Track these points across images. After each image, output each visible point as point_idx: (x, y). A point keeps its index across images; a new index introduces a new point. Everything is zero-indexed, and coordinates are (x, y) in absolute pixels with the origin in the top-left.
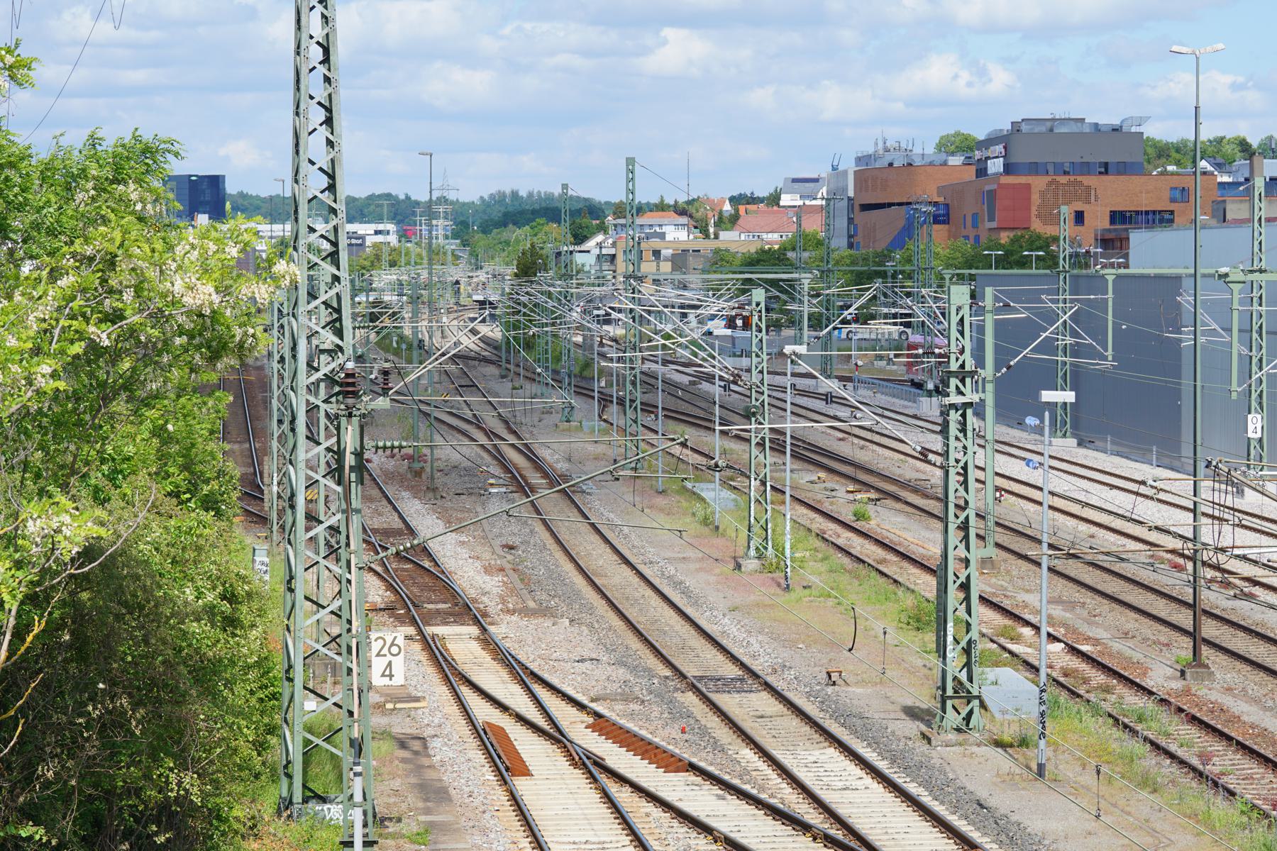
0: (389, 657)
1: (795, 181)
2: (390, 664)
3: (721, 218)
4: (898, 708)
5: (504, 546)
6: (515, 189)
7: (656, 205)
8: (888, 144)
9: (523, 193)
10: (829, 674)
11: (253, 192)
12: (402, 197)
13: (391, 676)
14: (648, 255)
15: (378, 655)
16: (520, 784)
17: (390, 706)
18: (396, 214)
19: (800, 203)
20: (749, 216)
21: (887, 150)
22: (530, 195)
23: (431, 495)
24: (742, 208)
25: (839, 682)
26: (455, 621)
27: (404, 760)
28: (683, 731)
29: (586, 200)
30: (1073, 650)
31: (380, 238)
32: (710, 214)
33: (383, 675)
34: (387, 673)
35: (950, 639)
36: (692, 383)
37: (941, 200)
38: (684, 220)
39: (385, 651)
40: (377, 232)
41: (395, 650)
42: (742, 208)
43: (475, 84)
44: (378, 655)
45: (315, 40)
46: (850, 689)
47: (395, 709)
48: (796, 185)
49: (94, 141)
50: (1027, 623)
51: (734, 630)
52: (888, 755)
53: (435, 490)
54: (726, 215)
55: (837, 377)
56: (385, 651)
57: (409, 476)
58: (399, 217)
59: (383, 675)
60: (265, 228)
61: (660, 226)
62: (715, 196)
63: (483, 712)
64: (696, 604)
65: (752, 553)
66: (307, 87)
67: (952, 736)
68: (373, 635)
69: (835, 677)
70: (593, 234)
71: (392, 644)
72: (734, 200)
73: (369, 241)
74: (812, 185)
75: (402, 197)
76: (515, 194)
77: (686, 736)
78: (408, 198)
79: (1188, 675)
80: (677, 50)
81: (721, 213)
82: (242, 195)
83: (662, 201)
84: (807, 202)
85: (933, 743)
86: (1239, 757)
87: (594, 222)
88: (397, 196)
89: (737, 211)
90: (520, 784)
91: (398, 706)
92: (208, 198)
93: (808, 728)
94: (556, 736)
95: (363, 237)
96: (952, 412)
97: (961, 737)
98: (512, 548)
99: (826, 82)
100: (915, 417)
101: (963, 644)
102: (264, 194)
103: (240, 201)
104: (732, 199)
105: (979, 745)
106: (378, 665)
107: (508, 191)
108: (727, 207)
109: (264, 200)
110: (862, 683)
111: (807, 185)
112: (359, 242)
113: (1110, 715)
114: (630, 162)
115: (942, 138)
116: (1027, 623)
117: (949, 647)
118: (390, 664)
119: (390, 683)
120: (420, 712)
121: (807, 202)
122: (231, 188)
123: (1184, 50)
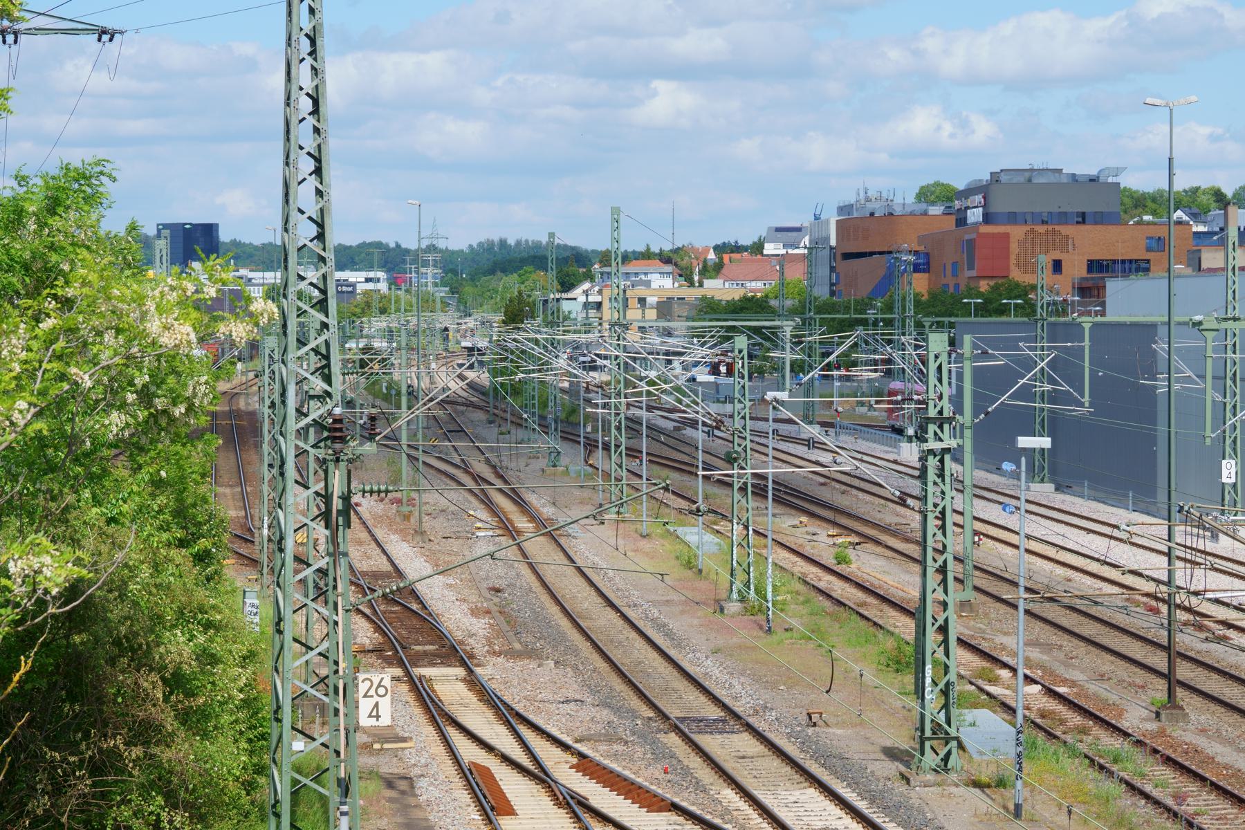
0: (376, 699)
1: (778, 230)
2: (377, 705)
4: (878, 749)
6: (503, 236)
8: (869, 194)
9: (511, 242)
10: (809, 716)
11: (246, 240)
12: (392, 245)
13: (378, 717)
14: (633, 303)
15: (365, 696)
16: (575, 760)
17: (377, 746)
19: (784, 252)
21: (868, 200)
22: (518, 243)
23: (419, 538)
24: (726, 257)
25: (820, 723)
26: (442, 663)
28: (666, 772)
29: (573, 248)
30: (1051, 692)
31: (370, 286)
32: (695, 262)
33: (370, 716)
34: (374, 713)
36: (677, 429)
37: (921, 248)
38: (669, 268)
39: (372, 692)
40: (368, 280)
41: (381, 691)
42: (726, 257)
43: (466, 134)
44: (365, 696)
46: (830, 730)
47: (382, 749)
48: (779, 235)
51: (716, 672)
54: (710, 263)
55: (819, 423)
56: (372, 692)
57: (398, 519)
58: (389, 265)
59: (370, 716)
61: (646, 274)
62: (699, 244)
63: (469, 752)
64: (679, 646)
65: (735, 596)
66: (297, 137)
67: (930, 777)
68: (361, 676)
69: (815, 718)
71: (379, 685)
72: (719, 249)
73: (360, 288)
74: (795, 234)
75: (392, 245)
76: (503, 243)
77: (669, 777)
78: (398, 246)
79: (1163, 717)
80: (666, 102)
81: (705, 261)
83: (648, 249)
84: (790, 251)
85: (912, 783)
86: (1213, 797)
89: (721, 259)
91: (386, 746)
93: (788, 769)
94: (540, 776)
95: (353, 285)
96: (930, 458)
97: (939, 778)
98: (498, 591)
101: (941, 685)
104: (716, 248)
105: (957, 785)
106: (365, 706)
107: (496, 239)
108: (712, 255)
109: (256, 248)
111: (790, 234)
112: (350, 289)
117: (928, 689)
118: (377, 705)
119: (377, 724)
120: (407, 752)
121: (790, 251)
122: (225, 236)
123: (1158, 102)
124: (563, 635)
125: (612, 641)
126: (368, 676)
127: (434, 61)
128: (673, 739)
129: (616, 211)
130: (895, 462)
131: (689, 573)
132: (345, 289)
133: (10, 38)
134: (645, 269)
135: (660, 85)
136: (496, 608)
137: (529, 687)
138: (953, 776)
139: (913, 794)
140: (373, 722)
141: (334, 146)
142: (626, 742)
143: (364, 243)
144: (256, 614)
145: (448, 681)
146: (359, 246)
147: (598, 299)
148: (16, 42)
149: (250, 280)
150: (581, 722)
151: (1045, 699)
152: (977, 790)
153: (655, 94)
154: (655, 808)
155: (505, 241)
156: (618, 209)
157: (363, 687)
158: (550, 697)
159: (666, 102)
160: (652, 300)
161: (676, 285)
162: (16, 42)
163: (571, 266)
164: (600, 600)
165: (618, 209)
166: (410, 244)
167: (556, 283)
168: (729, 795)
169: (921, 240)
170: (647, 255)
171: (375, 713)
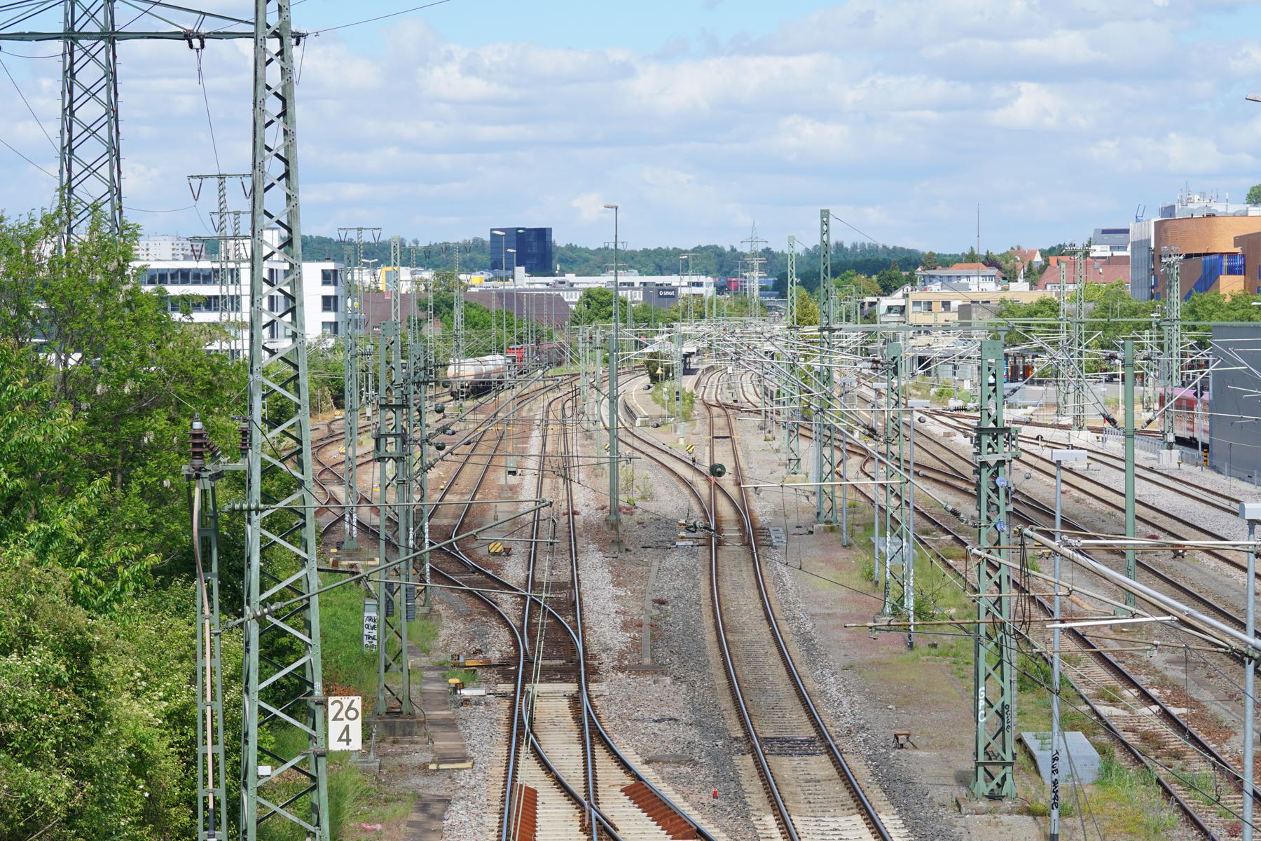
0: (346, 722)
1: (1105, 232)
2: (347, 728)
3: (1030, 269)
4: (952, 772)
5: (655, 601)
6: (840, 240)
7: (967, 257)
9: (848, 245)
10: (896, 736)
11: (581, 244)
12: (728, 249)
13: (348, 741)
14: (937, 307)
15: (335, 719)
16: (629, 782)
17: (433, 767)
18: (721, 266)
19: (1109, 254)
20: (1062, 267)
22: (855, 247)
23: (615, 548)
24: (1053, 260)
25: (908, 744)
27: (411, 824)
28: (715, 796)
29: (909, 251)
30: (1166, 715)
31: (696, 290)
32: (1019, 265)
33: (340, 740)
34: (344, 737)
35: (982, 703)
36: (947, 435)
37: (1238, 250)
38: (994, 271)
39: (342, 715)
41: (352, 714)
42: (1053, 260)
44: (335, 719)
45: (272, 91)
46: (916, 752)
47: (438, 770)
48: (1106, 237)
49: (416, 242)
50: (1133, 684)
52: (911, 823)
53: (619, 543)
54: (1035, 266)
55: (1089, 429)
56: (342, 715)
57: (605, 529)
59: (340, 740)
60: (637, 279)
62: (1026, 247)
64: (812, 662)
65: (888, 610)
66: (263, 140)
67: (983, 804)
69: (902, 739)
70: (902, 285)
71: (350, 708)
72: (1046, 254)
73: (684, 291)
74: (1122, 236)
75: (728, 249)
78: (733, 250)
80: (1029, 104)
81: (1030, 264)
82: (571, 248)
83: (972, 252)
84: (1116, 253)
85: (964, 810)
87: (904, 273)
88: (722, 249)
89: (1047, 261)
90: (629, 782)
92: (535, 250)
93: (847, 794)
95: (675, 289)
96: (984, 471)
97: (992, 805)
98: (662, 602)
99: (1172, 136)
100: (1151, 470)
101: (998, 707)
102: (592, 248)
103: (569, 254)
105: (1010, 813)
106: (335, 729)
108: (1038, 258)
110: (928, 747)
111: (1117, 236)
112: (672, 293)
113: (1159, 782)
114: (825, 214)
115: (1253, 189)
116: (1133, 684)
117: (981, 712)
118: (347, 728)
122: (559, 239)
124: (701, 650)
125: (749, 656)
126: (338, 698)
127: (803, 64)
128: (745, 763)
129: (825, 214)
130: (1151, 470)
131: (870, 584)
132: (666, 293)
133: (196, 43)
134: (965, 272)
135: (1027, 88)
136: (649, 621)
137: (629, 705)
138: (1008, 804)
139: (961, 822)
140: (342, 746)
141: (304, 153)
142: (696, 764)
143: (699, 247)
144: (373, 628)
145: (556, 698)
146: (655, 251)
147: (902, 303)
148: (203, 46)
149: (572, 285)
150: (663, 742)
151: (1157, 722)
152: (1030, 818)
153: (1019, 94)
154: (679, 835)
155: (842, 245)
156: (828, 211)
157: (333, 710)
158: (646, 715)
159: (1029, 104)
160: (955, 304)
161: (1000, 288)
162: (203, 46)
163: (890, 269)
164: (762, 613)
165: (828, 211)
166: (745, 248)
167: (877, 286)
168: (770, 820)
169: (1238, 241)
170: (971, 258)
171: (345, 737)
